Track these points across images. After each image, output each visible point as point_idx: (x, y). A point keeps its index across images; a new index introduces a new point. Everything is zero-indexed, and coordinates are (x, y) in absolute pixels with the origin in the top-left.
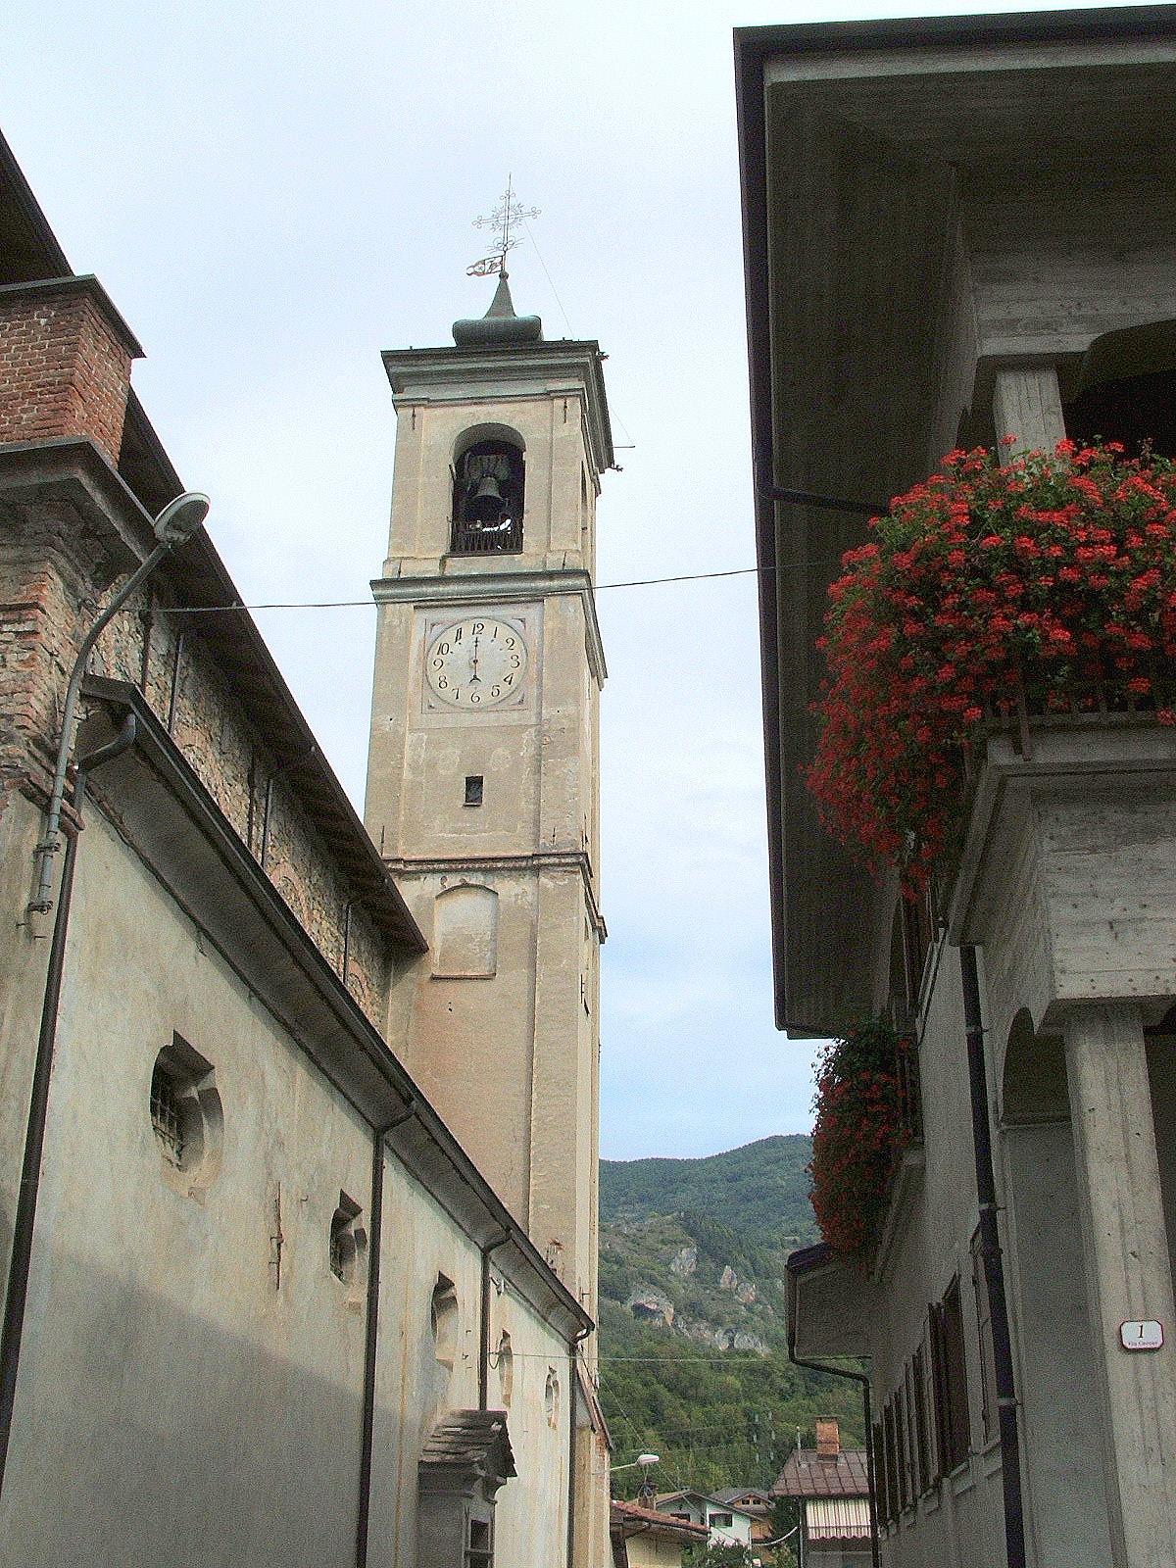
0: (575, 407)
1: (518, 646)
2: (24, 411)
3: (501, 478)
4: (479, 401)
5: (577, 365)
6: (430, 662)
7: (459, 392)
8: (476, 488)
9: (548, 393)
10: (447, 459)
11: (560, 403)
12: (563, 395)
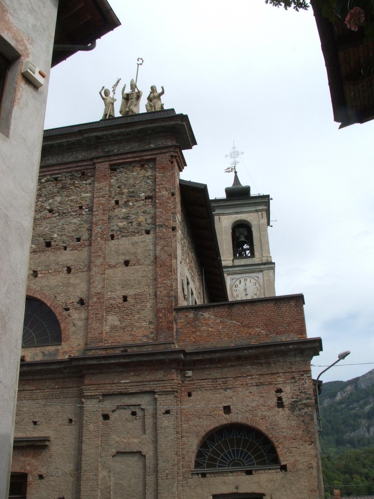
1: (257, 285)
2: (295, 326)
4: (237, 213)
6: (233, 290)
8: (238, 238)
10: (230, 231)
11: (260, 213)
12: (261, 211)
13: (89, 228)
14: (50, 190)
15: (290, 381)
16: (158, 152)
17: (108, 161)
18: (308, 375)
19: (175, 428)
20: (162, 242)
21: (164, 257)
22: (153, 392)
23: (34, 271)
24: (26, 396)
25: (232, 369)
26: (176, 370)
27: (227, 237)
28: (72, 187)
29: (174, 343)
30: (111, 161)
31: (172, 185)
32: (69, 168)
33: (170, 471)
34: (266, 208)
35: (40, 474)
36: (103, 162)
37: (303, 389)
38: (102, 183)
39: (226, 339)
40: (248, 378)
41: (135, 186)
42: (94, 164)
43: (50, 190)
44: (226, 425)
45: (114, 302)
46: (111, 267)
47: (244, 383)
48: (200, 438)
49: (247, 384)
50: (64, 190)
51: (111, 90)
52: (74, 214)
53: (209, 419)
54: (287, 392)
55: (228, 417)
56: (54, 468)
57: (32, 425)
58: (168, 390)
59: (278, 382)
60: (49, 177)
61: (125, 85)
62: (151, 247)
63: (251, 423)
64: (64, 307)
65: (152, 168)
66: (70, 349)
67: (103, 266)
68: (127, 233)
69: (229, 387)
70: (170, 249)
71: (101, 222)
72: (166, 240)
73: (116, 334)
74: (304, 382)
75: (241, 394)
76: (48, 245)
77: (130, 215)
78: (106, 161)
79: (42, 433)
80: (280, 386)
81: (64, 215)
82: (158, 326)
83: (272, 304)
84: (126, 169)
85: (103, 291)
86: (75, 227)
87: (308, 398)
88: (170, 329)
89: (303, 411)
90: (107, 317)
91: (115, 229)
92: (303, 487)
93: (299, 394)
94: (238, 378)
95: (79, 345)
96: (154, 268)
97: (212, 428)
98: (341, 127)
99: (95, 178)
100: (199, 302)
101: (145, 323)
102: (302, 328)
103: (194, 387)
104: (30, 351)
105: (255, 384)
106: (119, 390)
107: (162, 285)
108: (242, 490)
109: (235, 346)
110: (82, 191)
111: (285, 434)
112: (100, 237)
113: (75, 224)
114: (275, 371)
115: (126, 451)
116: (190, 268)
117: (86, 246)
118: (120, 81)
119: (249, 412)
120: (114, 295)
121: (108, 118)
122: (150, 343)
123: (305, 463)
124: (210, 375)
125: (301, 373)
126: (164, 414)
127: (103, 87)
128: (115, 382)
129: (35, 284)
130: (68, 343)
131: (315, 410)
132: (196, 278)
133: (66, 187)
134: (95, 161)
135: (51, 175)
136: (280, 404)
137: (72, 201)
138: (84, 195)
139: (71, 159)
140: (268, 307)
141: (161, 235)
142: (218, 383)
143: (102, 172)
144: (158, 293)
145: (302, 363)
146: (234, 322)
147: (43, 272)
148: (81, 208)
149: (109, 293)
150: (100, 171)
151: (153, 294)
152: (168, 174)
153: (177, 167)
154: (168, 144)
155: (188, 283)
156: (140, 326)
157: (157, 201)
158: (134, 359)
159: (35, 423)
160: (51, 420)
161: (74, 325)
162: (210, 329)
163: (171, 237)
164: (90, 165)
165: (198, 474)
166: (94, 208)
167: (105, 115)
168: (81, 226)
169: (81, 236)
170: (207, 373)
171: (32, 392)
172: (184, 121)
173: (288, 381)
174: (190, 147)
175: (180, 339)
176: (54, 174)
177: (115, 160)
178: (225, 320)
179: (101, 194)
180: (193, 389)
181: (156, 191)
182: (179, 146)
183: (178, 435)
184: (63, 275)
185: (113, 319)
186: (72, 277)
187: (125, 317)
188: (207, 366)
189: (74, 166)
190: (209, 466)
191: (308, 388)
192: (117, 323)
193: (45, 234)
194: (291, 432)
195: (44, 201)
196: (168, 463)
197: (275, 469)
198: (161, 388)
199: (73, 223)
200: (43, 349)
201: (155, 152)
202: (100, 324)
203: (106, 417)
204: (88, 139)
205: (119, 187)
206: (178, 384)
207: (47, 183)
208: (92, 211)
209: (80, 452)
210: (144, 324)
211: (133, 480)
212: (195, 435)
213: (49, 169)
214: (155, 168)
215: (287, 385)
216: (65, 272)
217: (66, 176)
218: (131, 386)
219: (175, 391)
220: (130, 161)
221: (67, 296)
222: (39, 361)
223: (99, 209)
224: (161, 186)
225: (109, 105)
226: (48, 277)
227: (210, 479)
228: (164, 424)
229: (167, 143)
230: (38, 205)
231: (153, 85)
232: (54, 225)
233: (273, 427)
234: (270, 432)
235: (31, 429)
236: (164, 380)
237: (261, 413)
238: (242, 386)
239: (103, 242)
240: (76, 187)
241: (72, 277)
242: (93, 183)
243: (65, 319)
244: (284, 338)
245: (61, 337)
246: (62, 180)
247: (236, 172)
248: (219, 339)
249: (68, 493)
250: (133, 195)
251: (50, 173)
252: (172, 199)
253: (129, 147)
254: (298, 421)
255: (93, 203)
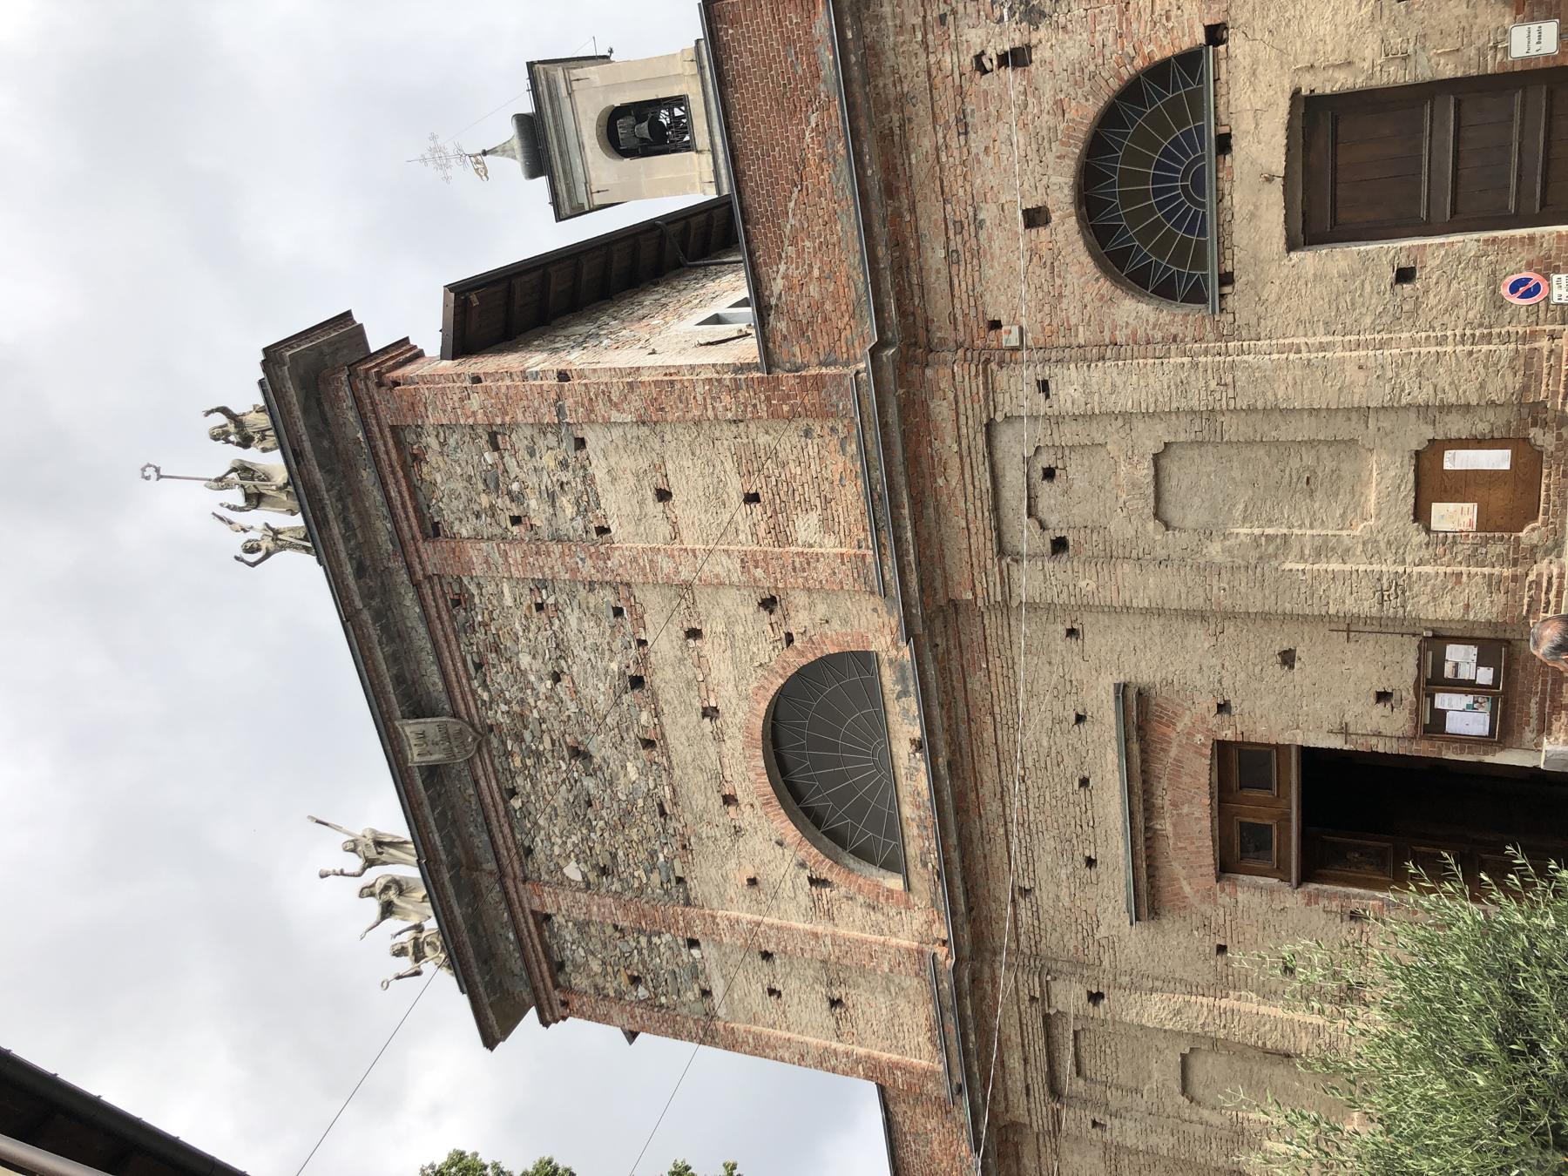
0: (577, 73)
2: (791, 23)
3: (634, 122)
4: (581, 146)
9: (569, 94)
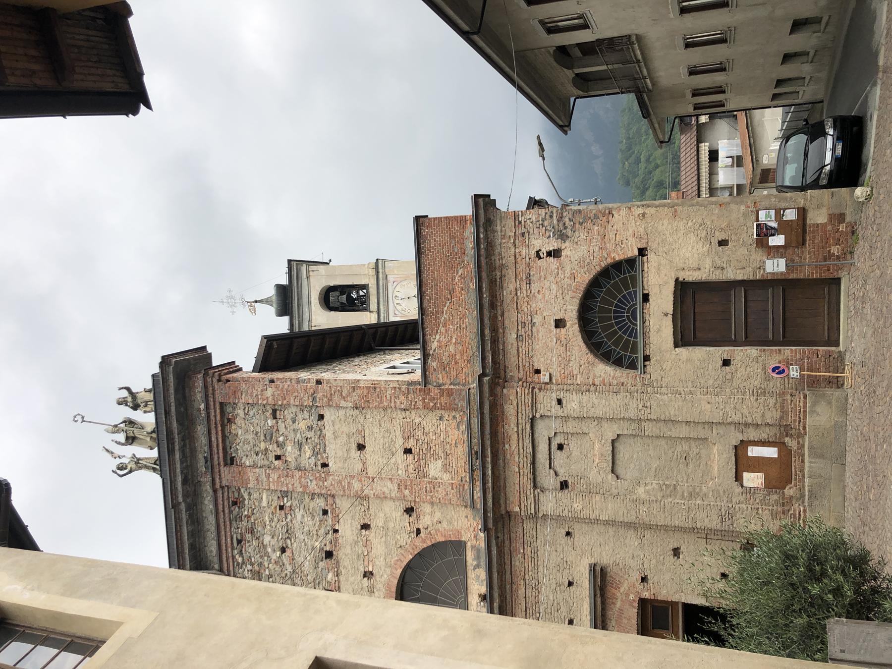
4: (309, 303)
5: (297, 267)
7: (306, 310)
9: (307, 277)
11: (311, 273)
12: (308, 272)
13: (310, 497)
14: (254, 551)
15: (527, 239)
16: (212, 399)
17: (219, 468)
18: (520, 215)
19: (582, 394)
20: (336, 398)
21: (355, 397)
22: (533, 420)
23: (365, 576)
24: (534, 595)
25: (506, 315)
26: (504, 388)
27: (340, 317)
28: (252, 519)
29: (469, 389)
30: (219, 464)
31: (259, 381)
32: (225, 522)
33: (639, 403)
34: (305, 265)
35: (640, 580)
36: (220, 475)
37: (538, 223)
38: (249, 477)
39: (467, 321)
40: (519, 294)
41: (257, 433)
42: (222, 487)
43: (254, 551)
44: (580, 326)
45: (412, 466)
46: (364, 470)
47: (525, 300)
48: (597, 360)
49: (528, 297)
50: (255, 530)
51: (118, 461)
52: (289, 517)
53: (571, 347)
54: (541, 243)
55: (570, 322)
56: (632, 561)
57: (573, 588)
58: (530, 399)
59: (527, 256)
60: (236, 552)
61: (112, 440)
62: (341, 412)
63: (579, 293)
64: (415, 536)
65: (234, 409)
66: (472, 529)
67: (363, 479)
68: (320, 445)
69: (530, 319)
70: (345, 389)
71: (303, 479)
72: (333, 393)
73: (454, 465)
74: (528, 221)
75: (540, 304)
76: (329, 555)
77: (296, 440)
78: (219, 471)
79: (584, 574)
80: (533, 253)
81: (290, 532)
82: (446, 408)
83: (424, 259)
84: (233, 444)
85: (396, 480)
86: (308, 517)
87: (551, 217)
88: (450, 393)
89: (567, 222)
90: (430, 476)
91: (314, 461)
92: (670, 227)
93: (544, 228)
94: (519, 307)
95: (466, 517)
96: (369, 411)
97: (584, 344)
98: (148, 106)
99: (242, 487)
100: (418, 355)
101: (442, 425)
102: (459, 221)
103: (527, 365)
104: (472, 586)
105: (528, 285)
106: (529, 465)
107: (393, 401)
108: (670, 309)
109: (477, 309)
110: (259, 505)
111: (597, 248)
112: (323, 483)
113: (303, 516)
114: (513, 258)
115: (611, 461)
116: (373, 364)
117: (334, 502)
118: (107, 448)
119: (564, 295)
120: (402, 467)
121: (160, 466)
122: (467, 420)
123: (638, 223)
124: (512, 344)
125: (517, 224)
126: (562, 407)
127: (113, 471)
128: (517, 470)
129: (382, 576)
130: (463, 532)
131: (568, 208)
132: (387, 357)
133: (252, 527)
134: (218, 486)
135: (233, 549)
136: (555, 254)
137: (271, 520)
138: (264, 503)
139: (212, 519)
140: (429, 263)
141: (326, 399)
142: (523, 334)
143: (234, 477)
144: (403, 406)
145: (503, 223)
146: (446, 308)
147: (366, 563)
148: (281, 508)
149: (400, 472)
150: (232, 480)
151: (403, 413)
152: (244, 386)
153: (235, 375)
154: (201, 385)
155: (394, 367)
156: (445, 433)
157: (280, 403)
158: (488, 443)
159: (570, 584)
160: (567, 562)
161: (440, 522)
162: (454, 341)
163: (330, 387)
164: (223, 494)
165: (645, 366)
166: (283, 490)
167: (154, 470)
168: (306, 508)
169: (319, 509)
170: (510, 347)
171: (527, 586)
172: (170, 361)
173: (527, 242)
174: (209, 356)
175: (464, 381)
176: (232, 543)
177: (219, 458)
178: (442, 320)
179: (265, 479)
180: (531, 367)
181: (266, 404)
182: (205, 370)
183: (591, 389)
184: (373, 535)
185: (435, 469)
186: (375, 522)
187: (432, 453)
188: (501, 348)
189: (222, 516)
190: (634, 350)
191: (537, 216)
192: (439, 463)
193: (314, 559)
194: (594, 240)
195: (269, 559)
196: (629, 405)
197: (643, 263)
198: (527, 409)
199: (302, 519)
200: (470, 568)
201: (212, 404)
202: (439, 487)
203: (564, 485)
204: (185, 496)
205: (257, 454)
206: (523, 387)
207: (244, 555)
208: (287, 492)
209: (611, 523)
210: (442, 427)
211: (651, 452)
212: (592, 367)
213: (224, 552)
214: (234, 404)
215: (532, 243)
216: (368, 532)
217: (236, 528)
218: (523, 448)
219: (532, 392)
220: (222, 437)
221: (400, 531)
222: (486, 573)
223: (285, 483)
224: (259, 397)
225: (138, 464)
226: (374, 556)
227: (652, 351)
228: (575, 407)
229: (199, 385)
230: (273, 567)
231: (115, 402)
232: (303, 547)
233: (585, 265)
234: (593, 268)
235: (578, 590)
236: (517, 403)
237: (566, 279)
238: (530, 303)
239: (331, 478)
240: (253, 514)
241: (375, 522)
242: (248, 490)
243: (431, 535)
244: (470, 244)
245: (455, 541)
246: (241, 534)
247: (256, 302)
248: (466, 330)
249: (667, 542)
250: (269, 436)
251: (230, 550)
252: (278, 383)
253: (202, 439)
254: (580, 230)
255: (276, 490)
